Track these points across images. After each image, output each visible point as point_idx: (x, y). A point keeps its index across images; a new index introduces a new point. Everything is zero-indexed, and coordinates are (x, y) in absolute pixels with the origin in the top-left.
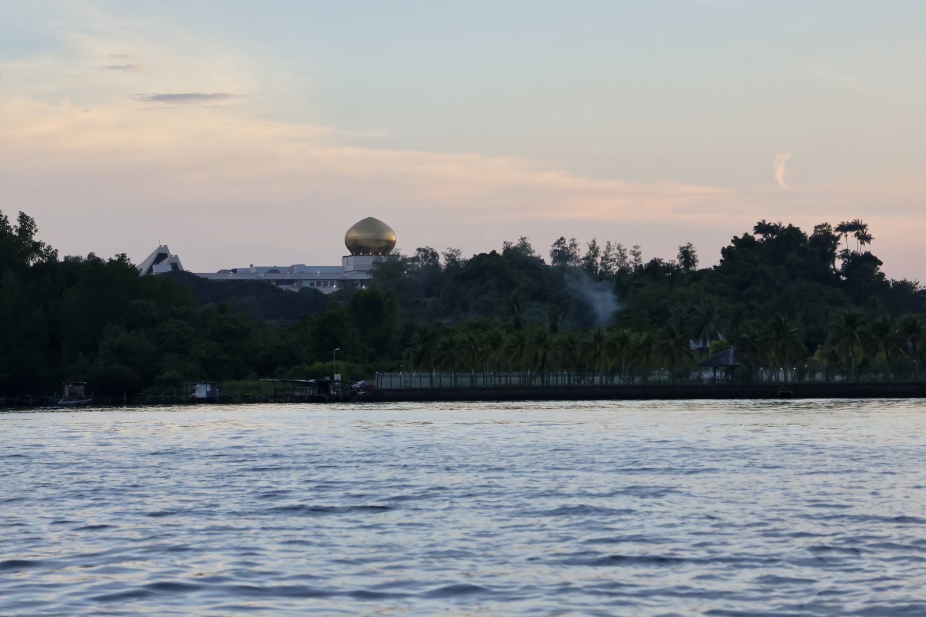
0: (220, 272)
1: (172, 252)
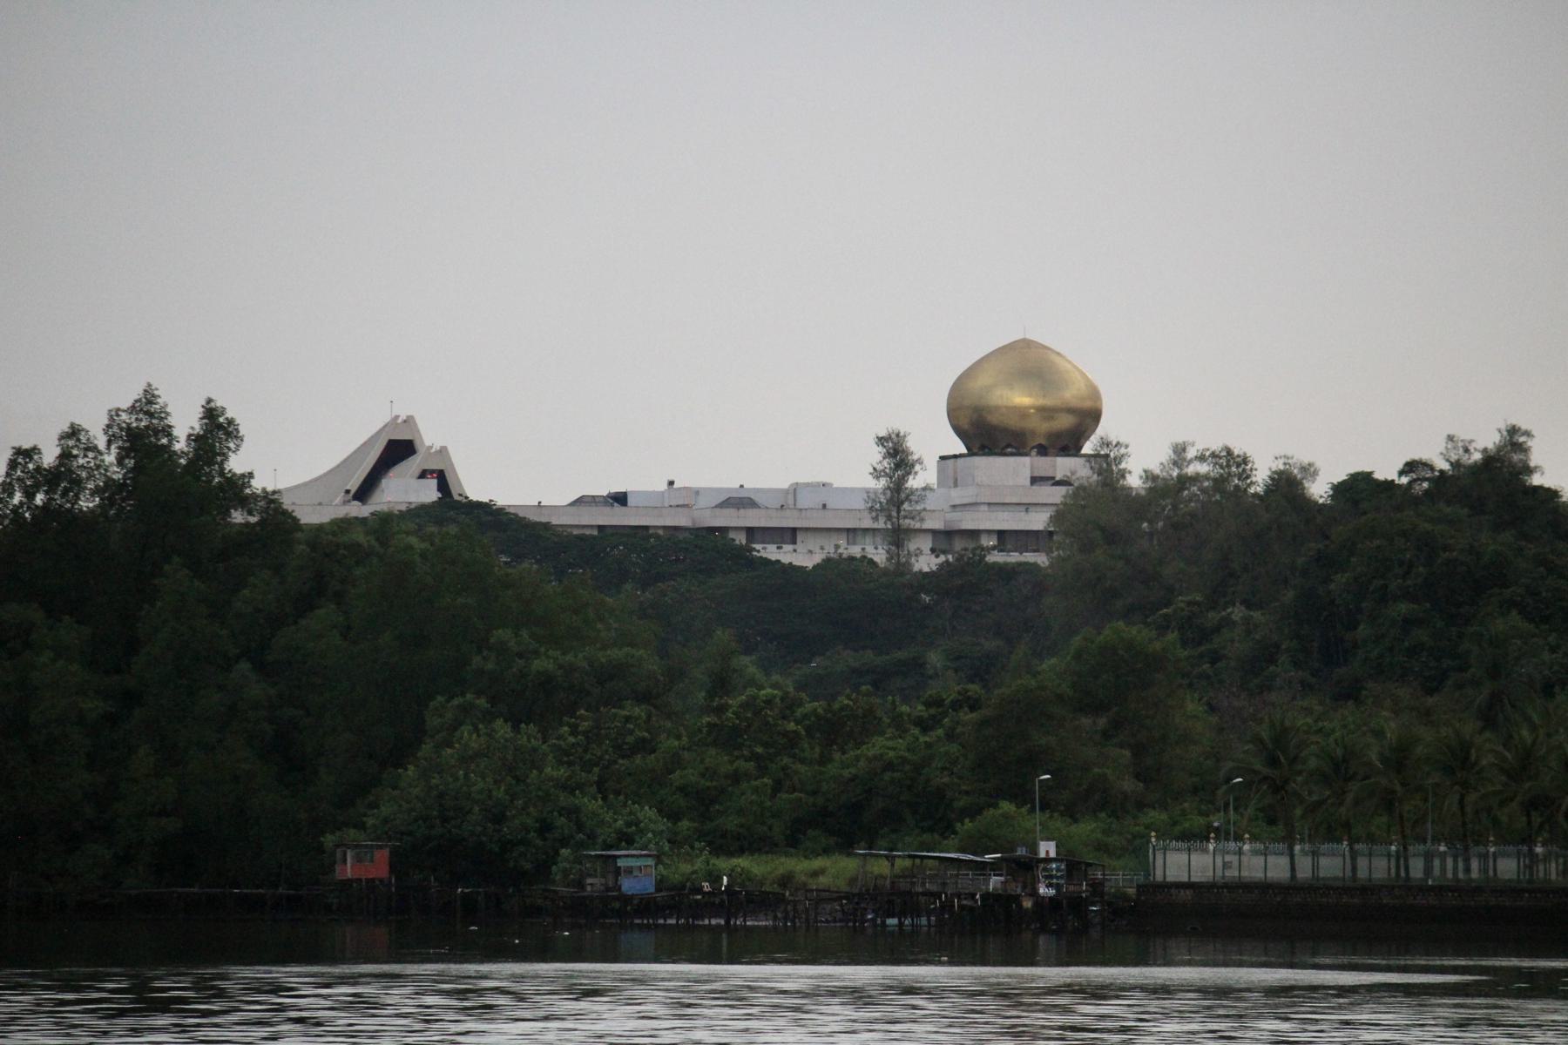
0: (580, 501)
1: (430, 437)
